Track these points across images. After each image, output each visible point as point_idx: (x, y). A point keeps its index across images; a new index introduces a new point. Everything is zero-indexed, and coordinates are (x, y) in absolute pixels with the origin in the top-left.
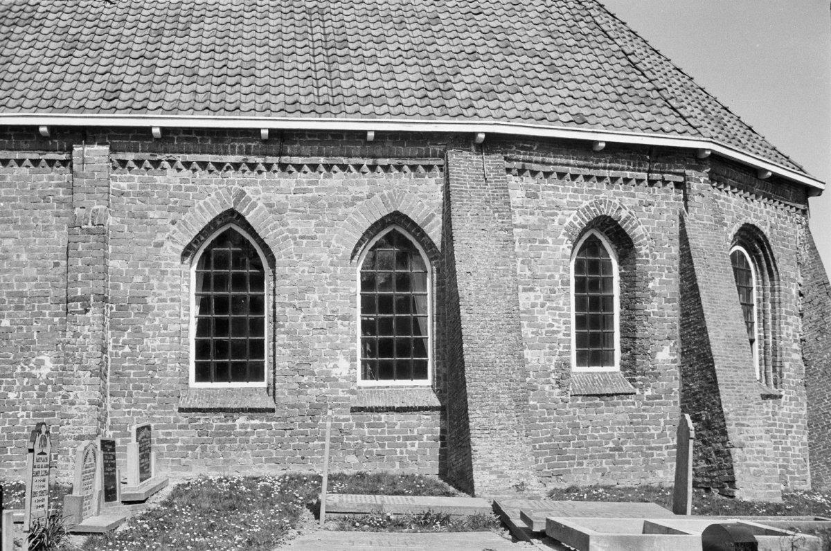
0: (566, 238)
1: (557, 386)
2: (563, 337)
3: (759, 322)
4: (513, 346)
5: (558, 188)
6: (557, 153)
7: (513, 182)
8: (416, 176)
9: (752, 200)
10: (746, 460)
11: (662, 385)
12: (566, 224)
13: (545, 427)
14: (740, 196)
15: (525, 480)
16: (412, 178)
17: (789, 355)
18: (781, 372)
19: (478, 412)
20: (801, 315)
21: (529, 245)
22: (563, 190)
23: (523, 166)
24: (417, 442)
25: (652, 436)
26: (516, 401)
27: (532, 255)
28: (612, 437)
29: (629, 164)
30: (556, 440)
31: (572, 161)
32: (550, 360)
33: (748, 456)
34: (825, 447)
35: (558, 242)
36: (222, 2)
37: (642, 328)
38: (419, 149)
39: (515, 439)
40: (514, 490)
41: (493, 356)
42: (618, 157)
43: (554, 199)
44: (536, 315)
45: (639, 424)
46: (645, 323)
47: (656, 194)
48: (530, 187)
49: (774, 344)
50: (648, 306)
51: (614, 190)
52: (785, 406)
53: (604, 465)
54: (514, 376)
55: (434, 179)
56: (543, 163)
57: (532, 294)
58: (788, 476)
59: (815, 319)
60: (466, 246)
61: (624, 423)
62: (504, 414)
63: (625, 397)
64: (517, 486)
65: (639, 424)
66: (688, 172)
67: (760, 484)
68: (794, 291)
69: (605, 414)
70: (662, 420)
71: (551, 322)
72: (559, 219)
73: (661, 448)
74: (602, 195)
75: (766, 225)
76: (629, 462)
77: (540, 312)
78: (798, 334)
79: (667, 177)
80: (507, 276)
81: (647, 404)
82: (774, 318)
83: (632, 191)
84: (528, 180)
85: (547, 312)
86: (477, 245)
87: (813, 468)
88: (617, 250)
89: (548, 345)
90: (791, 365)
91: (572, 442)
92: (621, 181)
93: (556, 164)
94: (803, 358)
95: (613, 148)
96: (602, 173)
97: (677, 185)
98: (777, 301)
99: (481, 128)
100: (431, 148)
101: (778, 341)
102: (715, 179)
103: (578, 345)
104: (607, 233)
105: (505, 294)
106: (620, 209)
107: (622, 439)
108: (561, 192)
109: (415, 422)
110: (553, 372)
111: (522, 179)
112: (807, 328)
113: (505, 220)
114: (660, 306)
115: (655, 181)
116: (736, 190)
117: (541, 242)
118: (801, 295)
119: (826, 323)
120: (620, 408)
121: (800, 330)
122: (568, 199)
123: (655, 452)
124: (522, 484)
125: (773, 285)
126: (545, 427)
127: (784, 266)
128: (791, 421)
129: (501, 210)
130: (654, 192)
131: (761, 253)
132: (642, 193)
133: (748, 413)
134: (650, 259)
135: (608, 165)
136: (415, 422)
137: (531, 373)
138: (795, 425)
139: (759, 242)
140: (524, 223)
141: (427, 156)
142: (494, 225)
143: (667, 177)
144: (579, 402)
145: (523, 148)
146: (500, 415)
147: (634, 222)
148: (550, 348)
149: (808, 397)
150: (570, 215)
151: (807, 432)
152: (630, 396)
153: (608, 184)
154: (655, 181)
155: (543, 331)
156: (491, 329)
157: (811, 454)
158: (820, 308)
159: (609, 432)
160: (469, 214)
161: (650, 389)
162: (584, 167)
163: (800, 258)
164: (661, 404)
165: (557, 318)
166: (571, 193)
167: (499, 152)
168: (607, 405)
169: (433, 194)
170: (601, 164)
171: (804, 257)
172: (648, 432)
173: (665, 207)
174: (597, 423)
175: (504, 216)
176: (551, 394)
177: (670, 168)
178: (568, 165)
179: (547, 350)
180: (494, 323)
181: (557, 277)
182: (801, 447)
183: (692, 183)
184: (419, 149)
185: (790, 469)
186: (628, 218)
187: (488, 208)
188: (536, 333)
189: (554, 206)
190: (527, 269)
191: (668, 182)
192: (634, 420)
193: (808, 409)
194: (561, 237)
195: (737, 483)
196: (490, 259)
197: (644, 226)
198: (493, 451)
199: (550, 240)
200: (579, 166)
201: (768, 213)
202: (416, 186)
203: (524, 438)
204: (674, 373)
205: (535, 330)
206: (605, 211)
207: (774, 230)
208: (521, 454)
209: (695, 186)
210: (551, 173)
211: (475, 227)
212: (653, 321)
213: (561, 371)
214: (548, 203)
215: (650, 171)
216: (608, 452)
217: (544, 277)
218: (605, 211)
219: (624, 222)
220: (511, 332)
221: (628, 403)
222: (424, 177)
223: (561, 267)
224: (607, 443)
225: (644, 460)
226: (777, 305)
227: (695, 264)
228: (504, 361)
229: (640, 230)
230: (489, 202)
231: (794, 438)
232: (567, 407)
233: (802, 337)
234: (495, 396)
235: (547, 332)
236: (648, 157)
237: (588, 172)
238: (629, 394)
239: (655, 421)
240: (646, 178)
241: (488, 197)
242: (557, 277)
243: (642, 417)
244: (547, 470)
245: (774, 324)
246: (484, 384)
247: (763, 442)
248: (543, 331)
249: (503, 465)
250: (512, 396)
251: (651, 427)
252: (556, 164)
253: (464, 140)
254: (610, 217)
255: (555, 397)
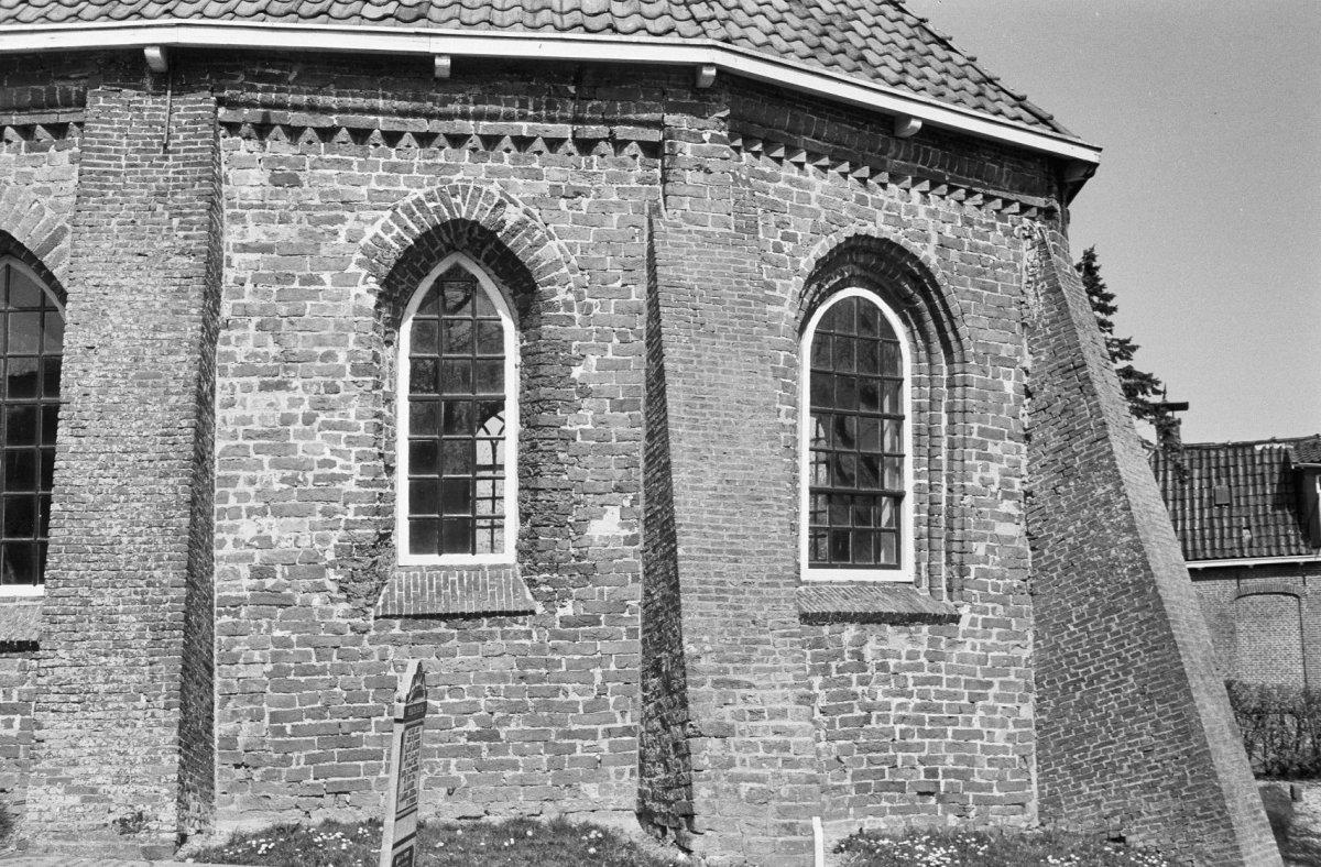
0: (364, 272)
1: (343, 596)
2: (355, 489)
3: (918, 455)
4: (166, 506)
5: (350, 164)
6: (343, 87)
7: (243, 153)
8: (30, 149)
9: (884, 186)
10: (731, 764)
11: (601, 593)
12: (365, 241)
13: (308, 685)
14: (844, 175)
15: (147, 810)
16: (23, 153)
17: (987, 526)
18: (962, 564)
19: (61, 653)
20: (1028, 437)
21: (275, 289)
22: (362, 166)
23: (266, 116)
24: (18, 718)
25: (573, 707)
26: (153, 629)
27: (283, 309)
28: (472, 709)
29: (524, 105)
30: (334, 714)
31: (380, 103)
32: (323, 540)
33: (738, 756)
34: (1068, 732)
35: (345, 280)
36: (556, 6)
37: (554, 467)
38: (33, 91)
39: (139, 714)
40: (114, 831)
41: (115, 531)
42: (497, 89)
43: (338, 186)
44: (292, 441)
45: (541, 679)
46: (561, 456)
47: (595, 169)
48: (281, 162)
49: (950, 500)
50: (571, 418)
51: (489, 163)
52: (970, 640)
53: (454, 772)
54: (157, 573)
55: (68, 152)
56: (312, 108)
57: (282, 397)
58: (971, 795)
59: (1053, 445)
60: (94, 291)
61: (504, 678)
62: (121, 660)
63: (508, 619)
64: (123, 822)
65: (541, 679)
66: (670, 119)
67: (763, 822)
68: (1009, 387)
69: (459, 658)
70: (598, 672)
71: (328, 455)
72: (349, 231)
73: (593, 735)
74: (460, 176)
75: (927, 239)
76: (515, 766)
77: (302, 435)
78: (1017, 482)
79: (621, 131)
80: (177, 353)
81: (561, 636)
82: (952, 446)
83: (536, 165)
84: (280, 147)
85: (319, 435)
86: (119, 287)
87: (1045, 776)
88: (513, 296)
89: (319, 506)
90: (990, 550)
91: (373, 720)
92: (506, 142)
93: (344, 110)
94: (1028, 534)
95: (465, 67)
96: (459, 126)
97: (652, 150)
98: (959, 407)
99: (153, 36)
100: (58, 86)
101: (957, 496)
102: (745, 132)
103: (414, 508)
104: (487, 261)
105: (167, 393)
106: (501, 204)
107: (498, 715)
108: (356, 172)
109: (15, 674)
110: (332, 565)
111: (264, 146)
112: (1036, 466)
113: (194, 233)
114: (599, 417)
115: (595, 142)
116: (825, 161)
117: (306, 281)
118: (1029, 394)
119: (1075, 454)
120: (497, 644)
121: (1024, 471)
122: (373, 185)
123: (578, 742)
124: (140, 817)
125: (952, 374)
126: (308, 685)
127: (974, 328)
128: (986, 673)
129: (187, 211)
130: (589, 166)
131: (921, 303)
132: (556, 171)
133: (756, 655)
134: (576, 314)
135: (472, 108)
136: (15, 674)
137: (278, 568)
138: (996, 681)
139: (915, 280)
140: (264, 240)
141: (53, 105)
142: (167, 244)
143: (621, 131)
144: (396, 631)
145: (261, 78)
146: (112, 661)
147: (538, 234)
148: (324, 513)
149: (1037, 619)
150: (374, 221)
151: (1033, 697)
152: (521, 619)
153: (474, 150)
154: (595, 142)
155: (310, 476)
156: (122, 469)
157: (1042, 745)
158: (1064, 421)
159: (467, 698)
160: (114, 221)
161: (570, 603)
162: (415, 114)
163: (1026, 312)
164: (594, 637)
165: (343, 446)
166: (381, 172)
167: (206, 88)
168: (464, 637)
169: (61, 184)
170: (451, 108)
171: (1035, 311)
172: (561, 698)
173: (615, 198)
174: (437, 677)
175: (192, 223)
176: (324, 614)
177: (625, 112)
178: (374, 111)
179: (318, 518)
180: (131, 458)
181: (342, 357)
182: (1012, 730)
183: (679, 144)
184: (33, 91)
185: (977, 779)
186: (522, 224)
187: (160, 208)
188: (293, 481)
189: (337, 201)
190: (270, 340)
191: (626, 143)
192: (530, 671)
193: (1037, 646)
194: (352, 268)
195: (697, 820)
196: (143, 319)
197: (562, 243)
198: (82, 743)
199: (326, 276)
200: (403, 114)
201: (933, 213)
202: (29, 169)
203: (160, 713)
204: (630, 567)
205: (289, 473)
206: (464, 209)
207: (953, 253)
208: (146, 749)
209: (687, 149)
210: (334, 130)
211: (121, 250)
212: (580, 452)
213: (351, 565)
214: (323, 195)
215: (577, 120)
216: (463, 741)
217: (311, 358)
218: (464, 209)
219: (513, 232)
220: (166, 475)
221: (516, 635)
222: (47, 150)
223: (352, 336)
224: (460, 723)
225: (550, 761)
226: (958, 417)
227: (664, 321)
228: (139, 539)
229: (552, 250)
230: (164, 195)
231: (994, 710)
232: (365, 643)
233: (1026, 487)
234: (107, 620)
235: (317, 478)
236: (572, 89)
237: (425, 126)
238: (517, 613)
239: (581, 671)
240: (570, 136)
241: (162, 183)
242: (342, 357)
243: (548, 663)
244: (311, 781)
245: (951, 458)
246: (84, 591)
247: (787, 723)
248: (310, 476)
249: (99, 773)
250: (146, 619)
251: (569, 687)
252: (344, 110)
253: (123, 66)
254: (476, 223)
255: (335, 620)
